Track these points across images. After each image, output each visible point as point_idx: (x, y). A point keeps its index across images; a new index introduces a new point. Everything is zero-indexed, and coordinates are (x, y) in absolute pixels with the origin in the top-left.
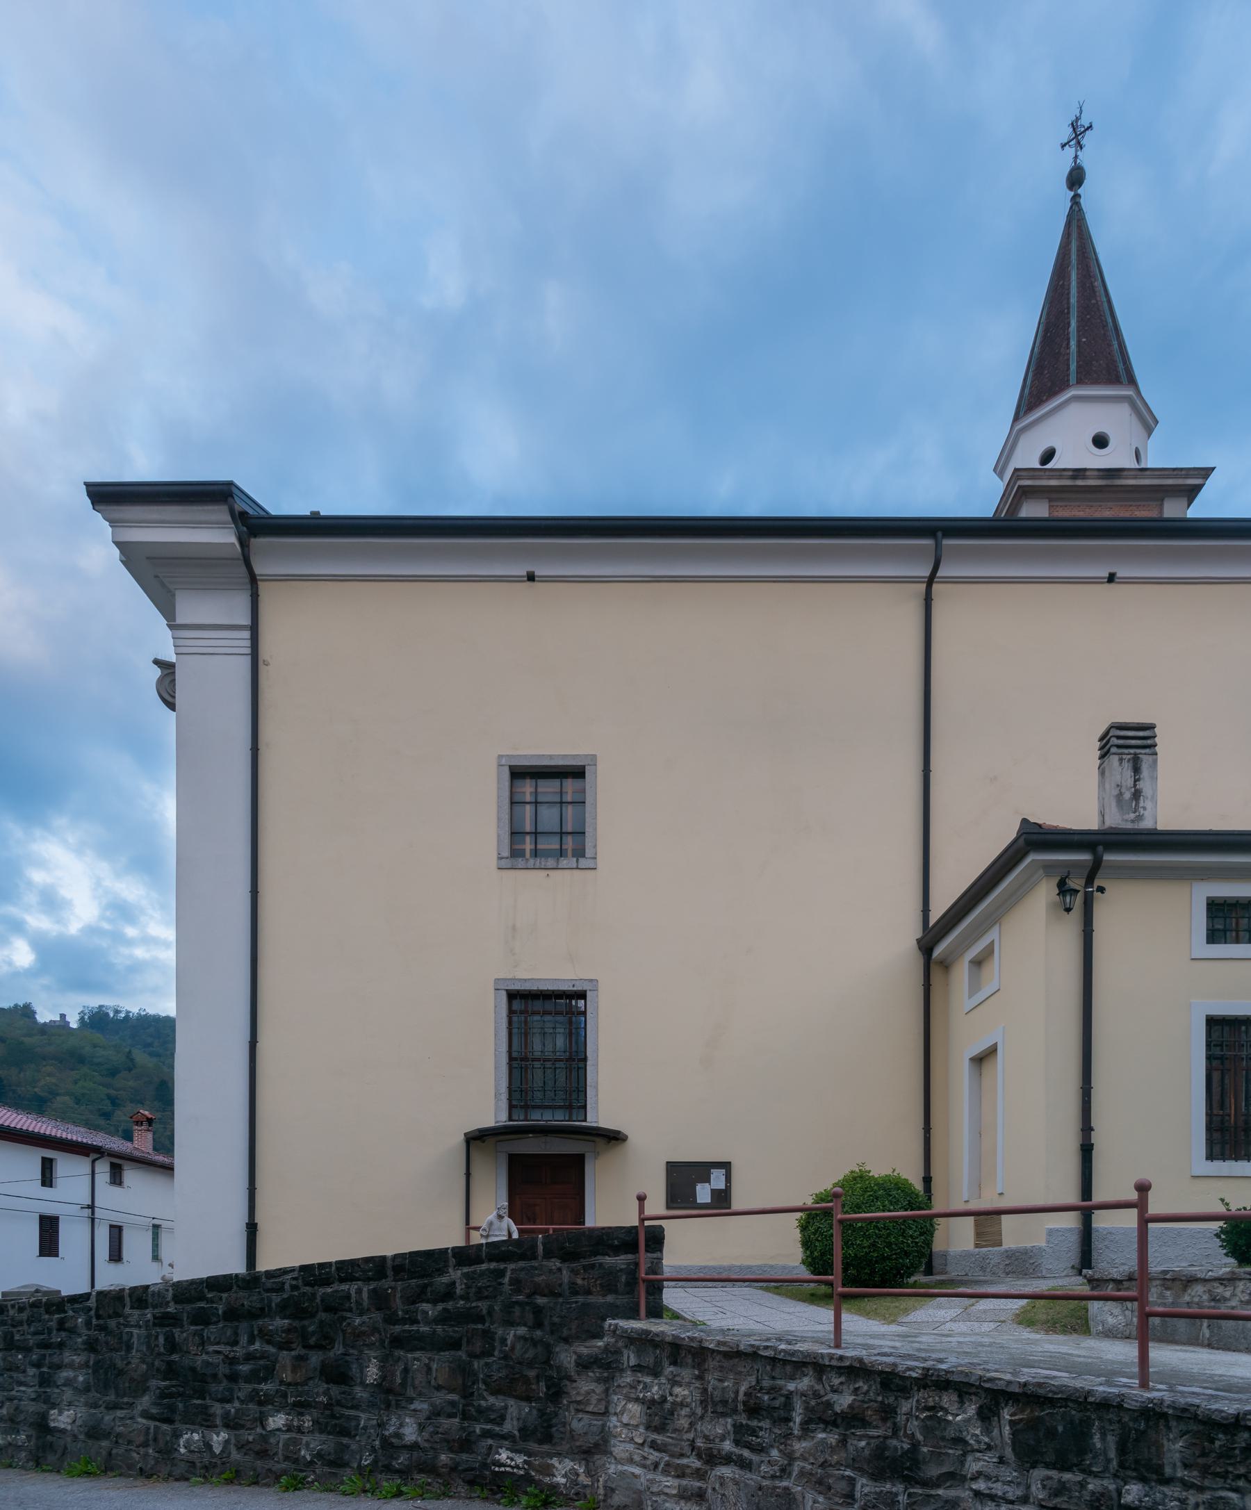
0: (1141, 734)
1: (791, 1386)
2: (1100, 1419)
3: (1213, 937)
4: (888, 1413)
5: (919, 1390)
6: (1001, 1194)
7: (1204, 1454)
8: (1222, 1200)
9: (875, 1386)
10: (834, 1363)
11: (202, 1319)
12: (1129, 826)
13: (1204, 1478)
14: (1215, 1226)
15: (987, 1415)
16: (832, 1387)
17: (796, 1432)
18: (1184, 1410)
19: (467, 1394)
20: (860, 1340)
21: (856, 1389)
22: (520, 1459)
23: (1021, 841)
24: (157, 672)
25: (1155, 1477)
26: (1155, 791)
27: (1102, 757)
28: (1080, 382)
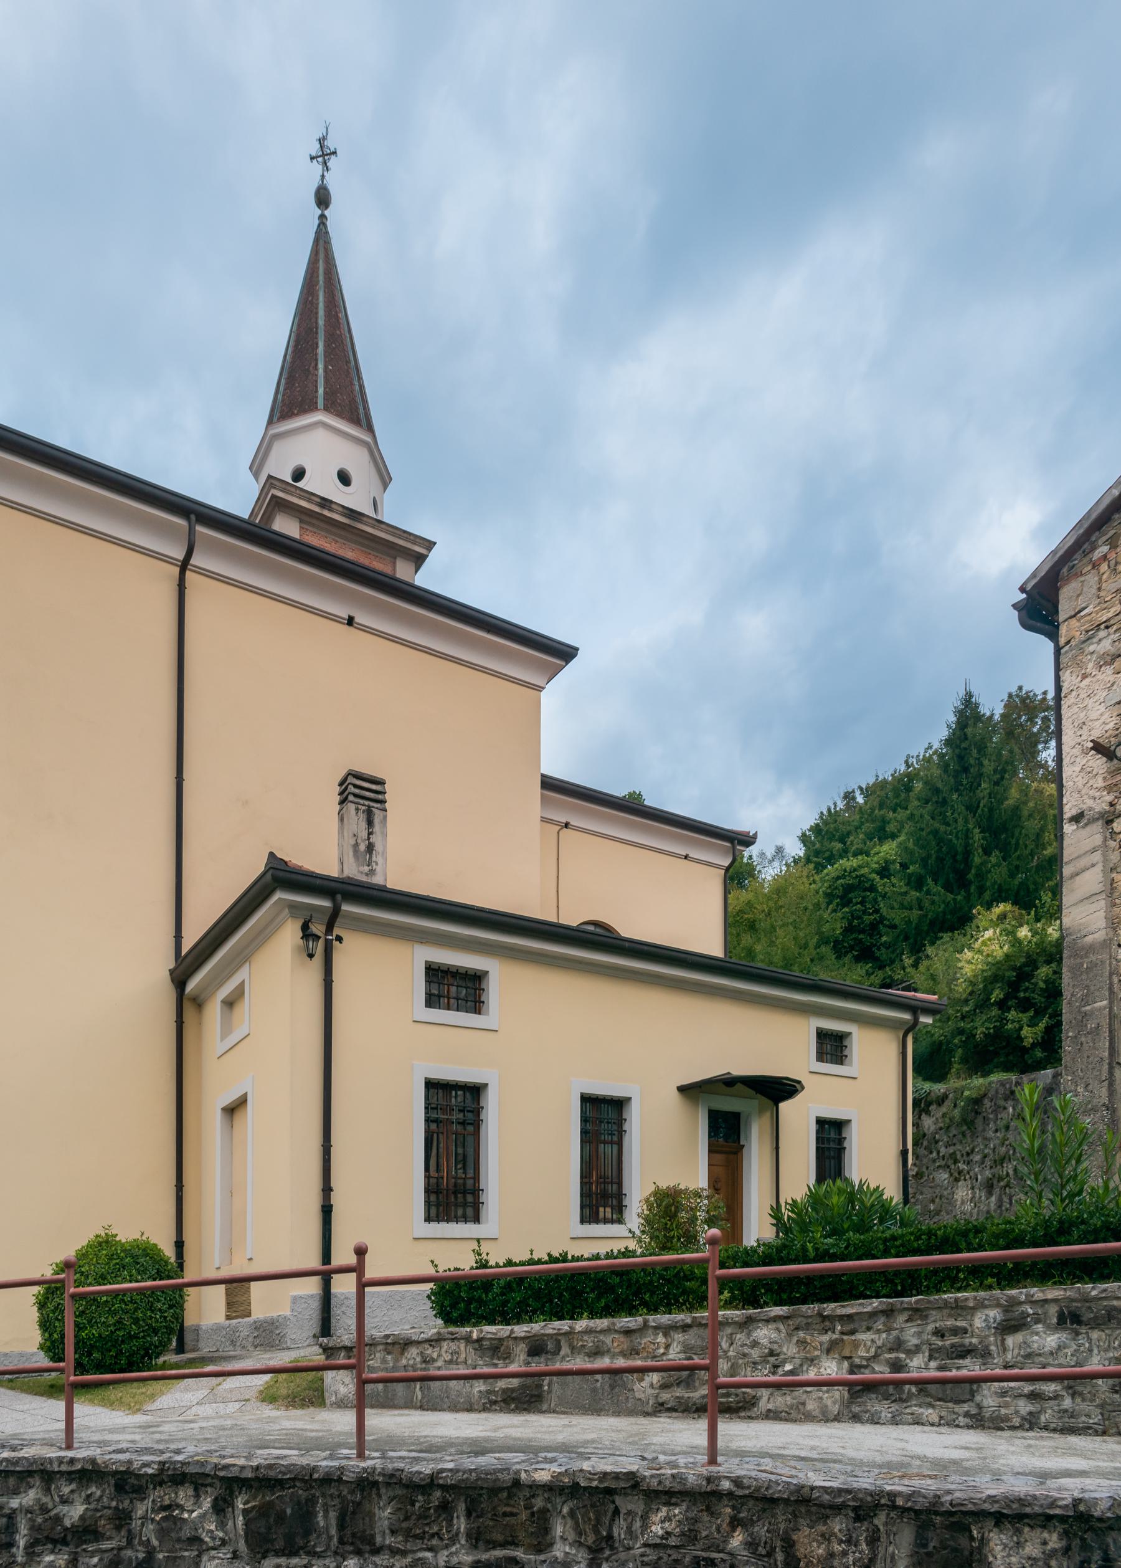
0: (374, 787)
1: (15, 1503)
2: (323, 1495)
3: (432, 1001)
4: (122, 1519)
5: (155, 1488)
6: (250, 1259)
7: (407, 1518)
8: (432, 1262)
9: (110, 1490)
10: (64, 1468)
12: (364, 879)
13: (406, 1541)
14: (428, 1287)
15: (221, 1508)
16: (61, 1497)
17: (19, 1559)
18: (392, 1476)
20: (96, 1437)
21: (89, 1496)
23: (269, 876)
25: (368, 1548)
26: (385, 847)
27: (342, 802)
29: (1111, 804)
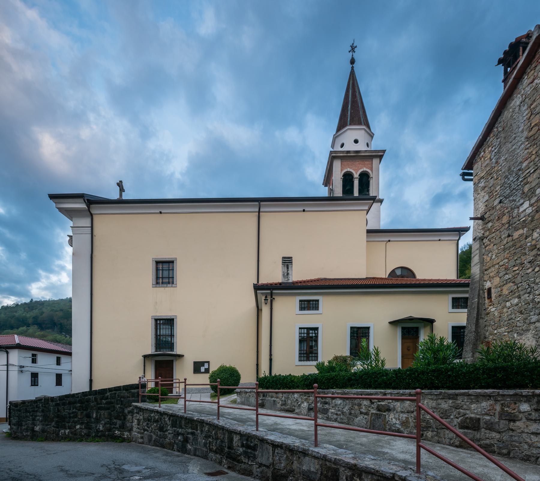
11: (64, 404)
15: (169, 419)
19: (111, 420)
22: (119, 433)
24: (68, 238)
28: (350, 124)
29: (483, 234)
